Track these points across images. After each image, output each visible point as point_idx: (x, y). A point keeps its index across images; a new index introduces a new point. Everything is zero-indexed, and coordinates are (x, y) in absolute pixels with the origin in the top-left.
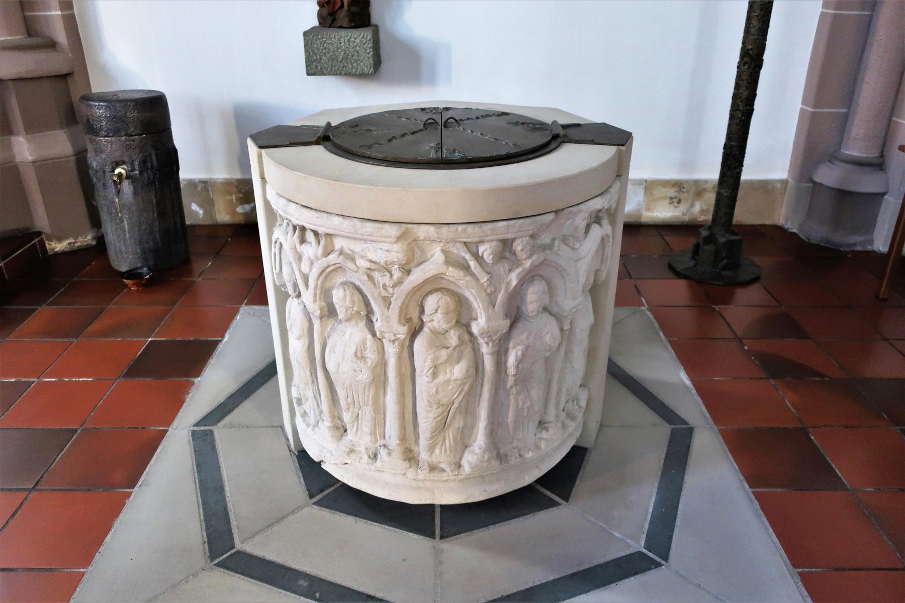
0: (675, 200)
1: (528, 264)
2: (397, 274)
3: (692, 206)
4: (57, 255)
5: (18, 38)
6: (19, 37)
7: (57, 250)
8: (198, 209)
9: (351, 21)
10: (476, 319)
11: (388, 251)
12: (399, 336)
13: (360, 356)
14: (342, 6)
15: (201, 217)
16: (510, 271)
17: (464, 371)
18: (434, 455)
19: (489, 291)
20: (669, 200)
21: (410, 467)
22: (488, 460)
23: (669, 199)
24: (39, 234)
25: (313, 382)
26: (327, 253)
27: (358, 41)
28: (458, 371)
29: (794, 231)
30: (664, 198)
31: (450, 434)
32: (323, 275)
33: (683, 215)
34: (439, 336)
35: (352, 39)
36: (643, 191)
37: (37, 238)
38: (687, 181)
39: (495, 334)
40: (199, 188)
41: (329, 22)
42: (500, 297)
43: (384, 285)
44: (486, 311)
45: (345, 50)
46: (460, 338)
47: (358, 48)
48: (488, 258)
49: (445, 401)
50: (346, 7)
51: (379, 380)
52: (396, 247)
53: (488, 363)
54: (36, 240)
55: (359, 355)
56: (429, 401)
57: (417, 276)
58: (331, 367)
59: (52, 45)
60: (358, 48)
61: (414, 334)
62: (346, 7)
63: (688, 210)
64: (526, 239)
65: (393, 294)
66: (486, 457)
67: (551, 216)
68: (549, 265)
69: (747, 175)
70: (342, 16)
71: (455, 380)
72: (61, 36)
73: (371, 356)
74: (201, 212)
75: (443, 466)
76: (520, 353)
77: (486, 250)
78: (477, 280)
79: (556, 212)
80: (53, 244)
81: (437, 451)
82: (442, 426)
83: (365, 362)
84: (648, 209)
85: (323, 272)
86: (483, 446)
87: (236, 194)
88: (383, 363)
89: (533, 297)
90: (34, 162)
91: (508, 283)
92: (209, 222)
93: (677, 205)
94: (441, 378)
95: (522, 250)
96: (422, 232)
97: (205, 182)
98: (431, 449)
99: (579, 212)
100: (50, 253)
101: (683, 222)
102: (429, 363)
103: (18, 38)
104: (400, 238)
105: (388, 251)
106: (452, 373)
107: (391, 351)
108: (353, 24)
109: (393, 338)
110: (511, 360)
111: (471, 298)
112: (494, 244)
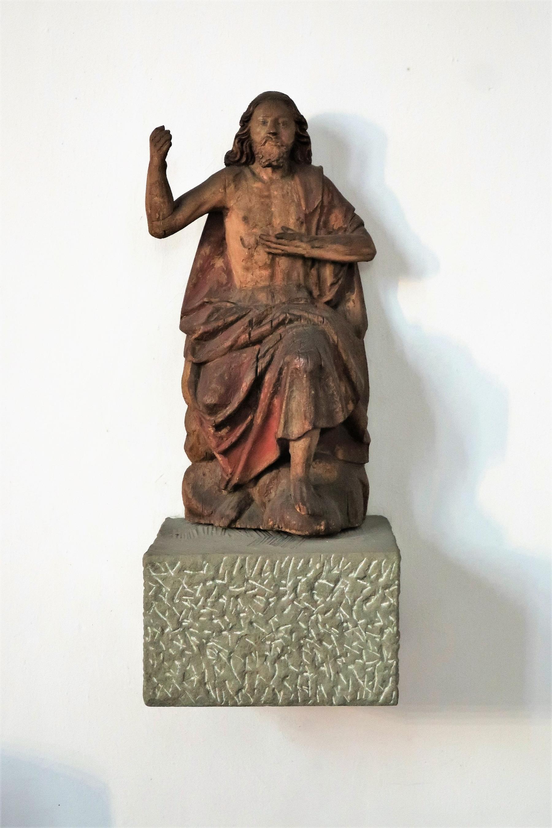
27: (345, 586)
47: (342, 614)
60: (342, 614)
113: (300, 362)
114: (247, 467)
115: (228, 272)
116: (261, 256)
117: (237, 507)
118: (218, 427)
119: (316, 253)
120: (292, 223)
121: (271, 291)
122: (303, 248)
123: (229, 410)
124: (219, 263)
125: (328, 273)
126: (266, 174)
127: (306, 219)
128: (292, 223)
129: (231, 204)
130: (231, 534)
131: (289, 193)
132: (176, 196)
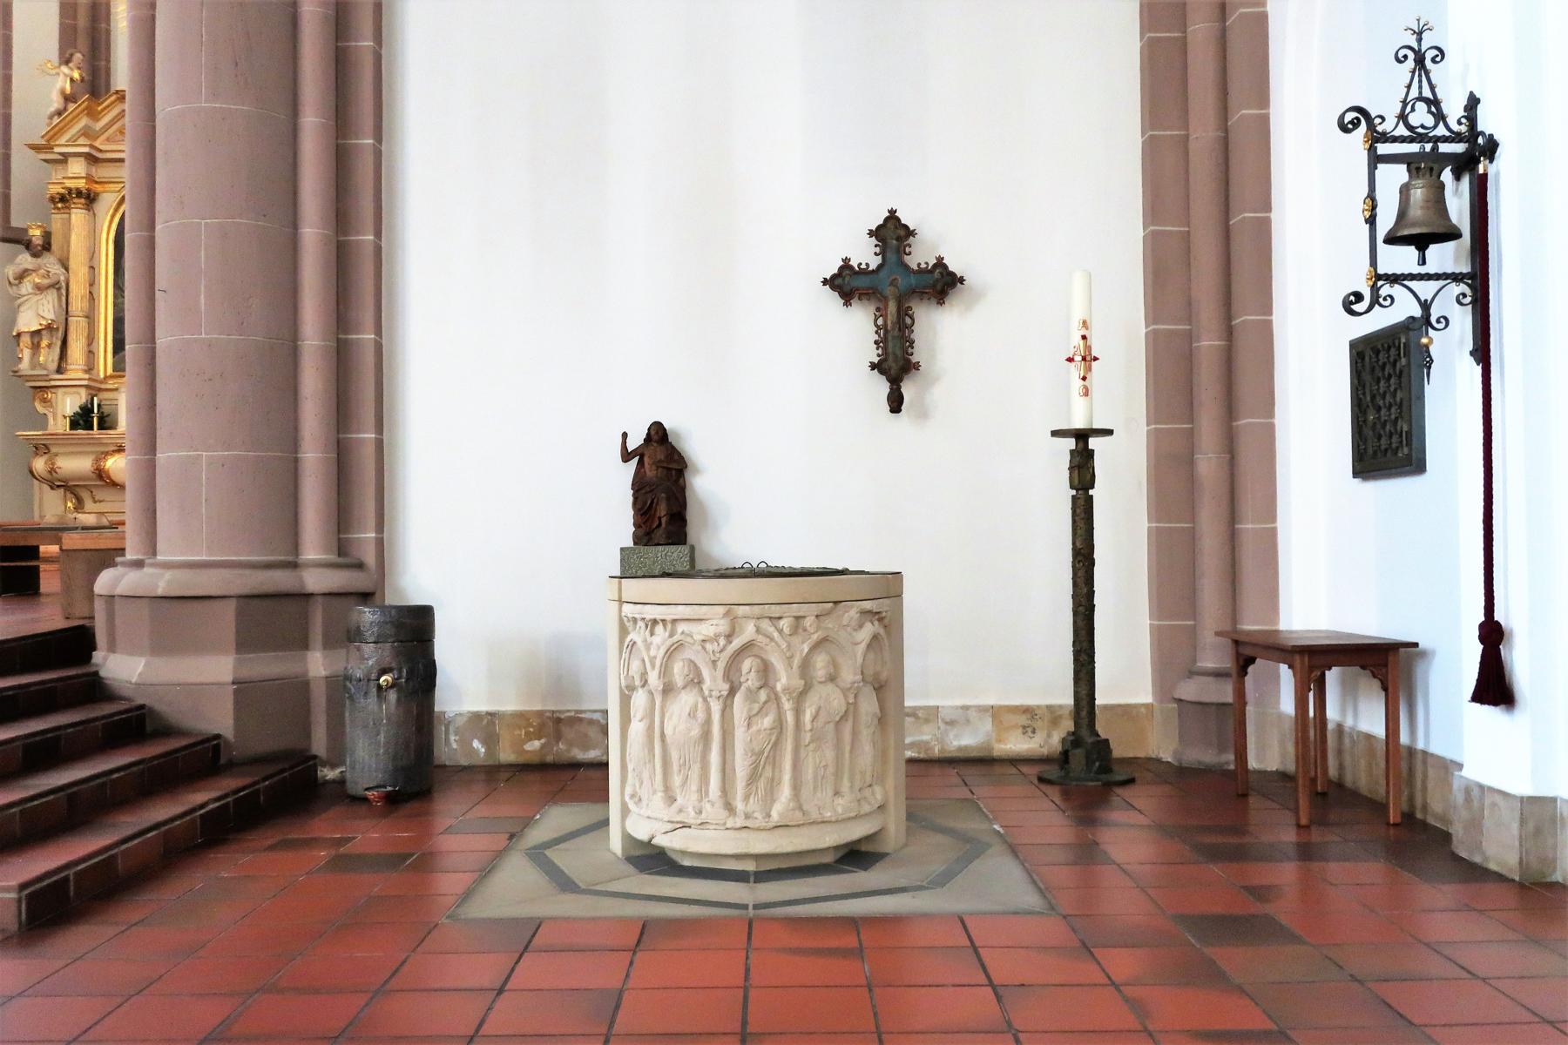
0: (1029, 730)
1: (815, 637)
2: (722, 642)
3: (1049, 735)
4: (326, 782)
5: (332, 557)
6: (331, 557)
7: (328, 778)
8: (480, 746)
9: (668, 538)
10: (780, 680)
11: (716, 625)
12: (722, 693)
13: (692, 714)
14: (660, 524)
15: (482, 755)
16: (803, 643)
17: (771, 722)
18: (749, 805)
19: (788, 655)
20: (1020, 730)
21: (730, 816)
22: (793, 810)
23: (1021, 728)
24: (315, 757)
25: (650, 761)
26: (671, 636)
27: (675, 555)
28: (767, 721)
29: (1169, 760)
30: (1015, 727)
31: (762, 784)
32: (667, 655)
33: (1041, 747)
34: (751, 695)
35: (669, 554)
36: (991, 719)
37: (286, 777)
38: (1038, 707)
39: (794, 692)
40: (485, 722)
41: (645, 541)
42: (796, 662)
43: (713, 651)
44: (787, 671)
45: (661, 564)
46: (768, 696)
47: (675, 562)
48: (786, 630)
49: (757, 750)
50: (663, 525)
51: (706, 736)
52: (722, 622)
53: (790, 718)
54: (311, 763)
55: (692, 715)
56: (745, 750)
57: (737, 643)
58: (668, 731)
59: (360, 566)
60: (675, 562)
61: (732, 692)
62: (663, 525)
63: (1046, 742)
64: (813, 618)
65: (719, 658)
66: (791, 805)
67: (831, 604)
68: (831, 641)
69: (1100, 700)
70: (660, 534)
71: (765, 730)
72: (370, 559)
73: (701, 715)
74: (483, 750)
75: (756, 815)
76: (814, 711)
77: (785, 624)
78: (779, 646)
79: (836, 603)
80: (326, 770)
81: (751, 801)
82: (753, 778)
83: (697, 720)
84: (999, 741)
85: (667, 652)
86: (789, 797)
87: (525, 728)
88: (708, 722)
89: (820, 663)
90: (327, 677)
91: (802, 650)
92: (490, 762)
93: (1032, 735)
94: (754, 728)
95: (810, 626)
96: (741, 610)
97: (491, 714)
98: (746, 798)
99: (852, 607)
100: (320, 781)
101: (1043, 755)
102: (745, 715)
103: (332, 557)
104: (726, 614)
105: (716, 625)
106: (762, 723)
107: (716, 707)
108: (670, 541)
109: (719, 695)
110: (808, 716)
111: (775, 663)
112: (791, 619)
113: (663, 495)
114: (650, 528)
115: (645, 472)
116: (654, 467)
117: (872, 623)
118: (642, 515)
119: (670, 466)
120: (662, 457)
121: (657, 477)
122: (665, 465)
123: (644, 510)
124: (643, 470)
125: (674, 472)
126: (655, 444)
127: (667, 457)
128: (662, 457)
129: (646, 452)
130: (448, 822)
131: (629, 793)
132: (629, 451)
